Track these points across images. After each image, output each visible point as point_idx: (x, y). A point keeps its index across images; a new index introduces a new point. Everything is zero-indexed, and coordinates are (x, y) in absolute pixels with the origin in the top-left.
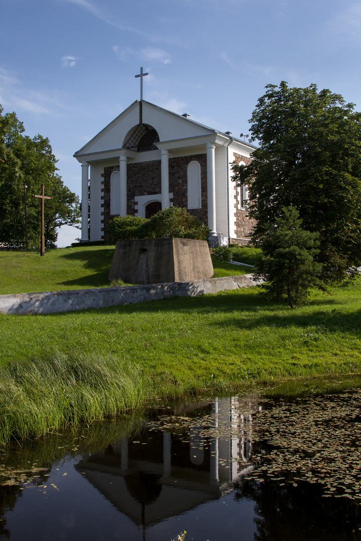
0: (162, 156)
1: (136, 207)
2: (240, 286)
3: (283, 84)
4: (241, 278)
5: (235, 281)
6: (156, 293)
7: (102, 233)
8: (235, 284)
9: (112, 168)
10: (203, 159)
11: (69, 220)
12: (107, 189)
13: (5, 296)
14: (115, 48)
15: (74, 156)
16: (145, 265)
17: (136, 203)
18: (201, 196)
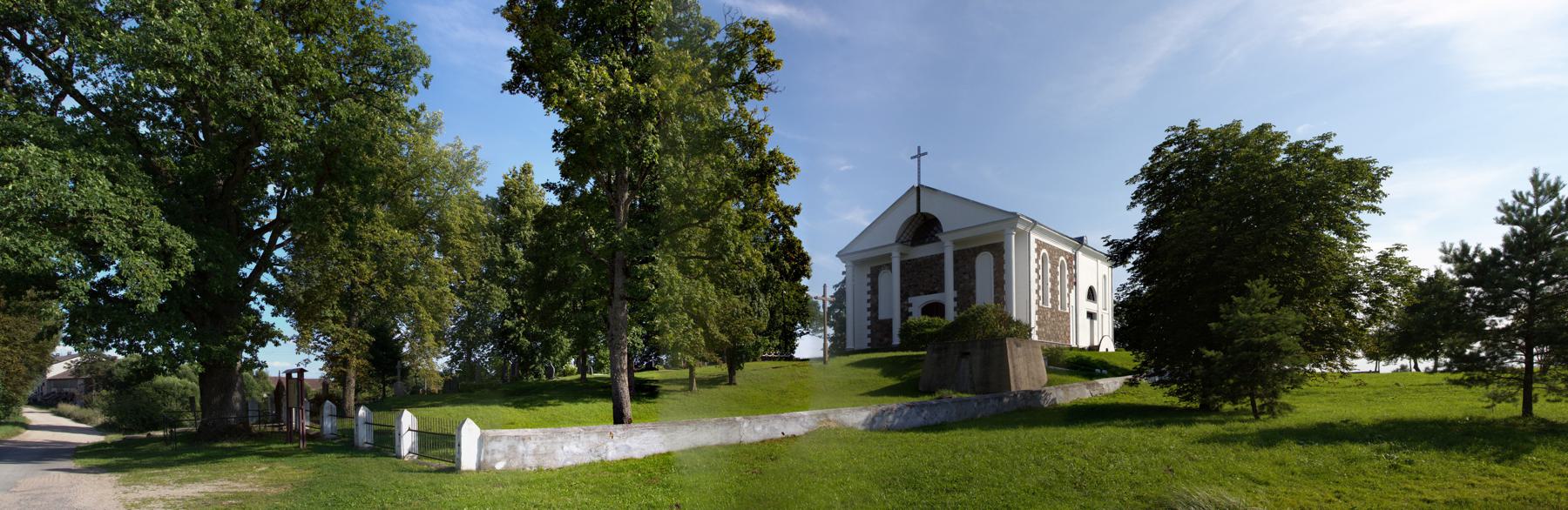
1: (910, 310)
4: (1093, 384)
7: (869, 340)
8: (1087, 391)
9: (881, 266)
10: (998, 251)
12: (874, 291)
13: (857, 408)
17: (911, 305)
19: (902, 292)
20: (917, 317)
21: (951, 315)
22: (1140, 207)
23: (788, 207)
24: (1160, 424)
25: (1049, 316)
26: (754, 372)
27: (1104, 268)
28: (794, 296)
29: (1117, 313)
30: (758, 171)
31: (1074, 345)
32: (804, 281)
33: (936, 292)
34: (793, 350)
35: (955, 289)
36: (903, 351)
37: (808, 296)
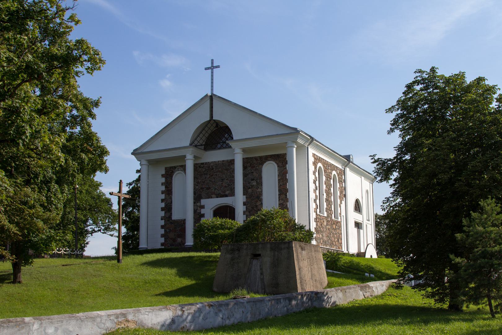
0: (236, 155)
1: (203, 211)
2: (366, 296)
3: (433, 70)
4: (366, 286)
5: (361, 291)
6: (297, 303)
7: (162, 240)
8: (361, 293)
9: (175, 167)
11: (103, 228)
12: (168, 191)
14: (136, 54)
15: (132, 154)
16: (258, 273)
17: (203, 207)
18: (278, 199)
19: (195, 193)
20: (208, 219)
21: (240, 219)
22: (397, 132)
23: (88, 99)
24: (426, 322)
25: (325, 224)
26: (41, 270)
27: (367, 184)
28: (87, 191)
29: (377, 225)
30: (62, 56)
31: (345, 251)
32: (99, 176)
33: (226, 196)
34: (82, 249)
35: (244, 195)
36: (197, 251)
37: (101, 192)
